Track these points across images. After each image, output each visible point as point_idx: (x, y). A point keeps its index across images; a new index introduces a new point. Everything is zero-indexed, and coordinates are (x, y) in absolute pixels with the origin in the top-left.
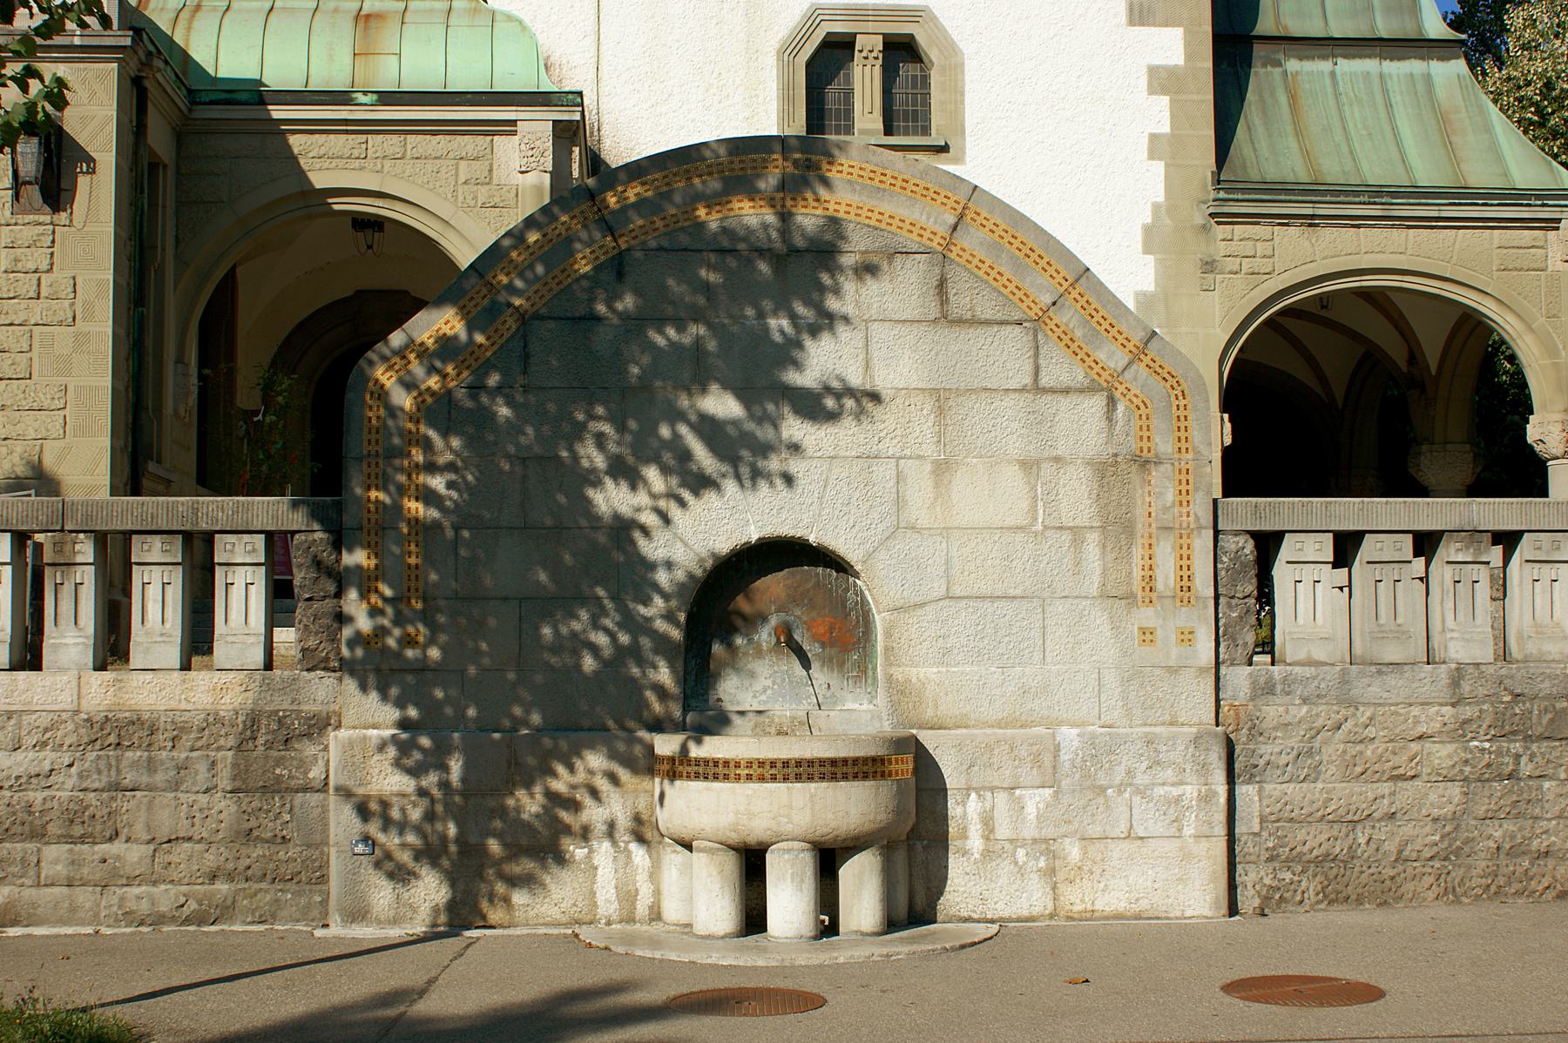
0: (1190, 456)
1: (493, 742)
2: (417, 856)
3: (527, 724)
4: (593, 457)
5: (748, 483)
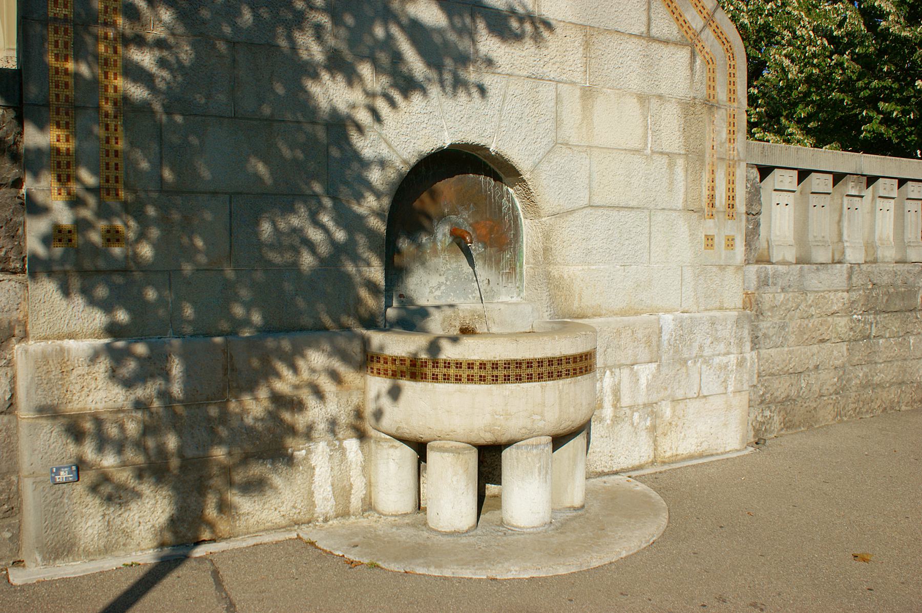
0: (735, 104)
1: (215, 345)
2: (140, 474)
3: (247, 322)
4: (312, 49)
5: (449, 89)
